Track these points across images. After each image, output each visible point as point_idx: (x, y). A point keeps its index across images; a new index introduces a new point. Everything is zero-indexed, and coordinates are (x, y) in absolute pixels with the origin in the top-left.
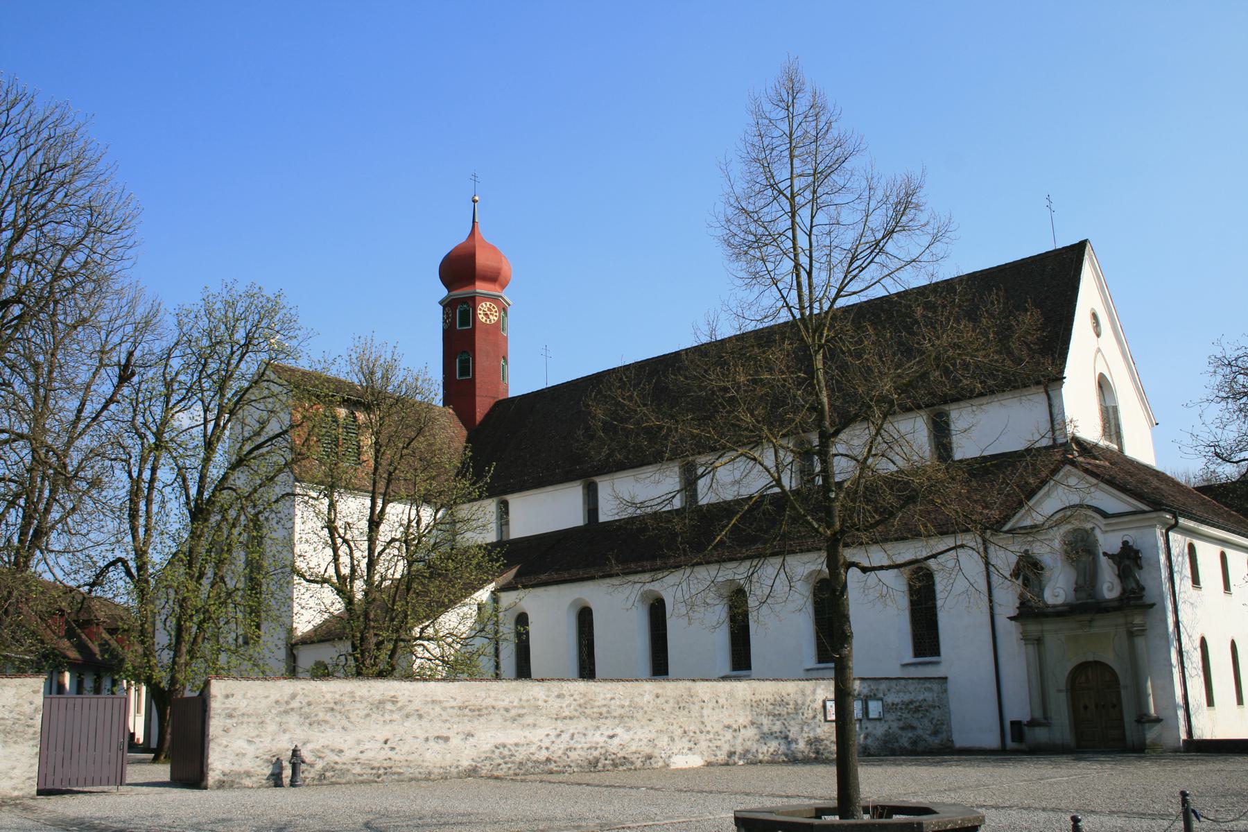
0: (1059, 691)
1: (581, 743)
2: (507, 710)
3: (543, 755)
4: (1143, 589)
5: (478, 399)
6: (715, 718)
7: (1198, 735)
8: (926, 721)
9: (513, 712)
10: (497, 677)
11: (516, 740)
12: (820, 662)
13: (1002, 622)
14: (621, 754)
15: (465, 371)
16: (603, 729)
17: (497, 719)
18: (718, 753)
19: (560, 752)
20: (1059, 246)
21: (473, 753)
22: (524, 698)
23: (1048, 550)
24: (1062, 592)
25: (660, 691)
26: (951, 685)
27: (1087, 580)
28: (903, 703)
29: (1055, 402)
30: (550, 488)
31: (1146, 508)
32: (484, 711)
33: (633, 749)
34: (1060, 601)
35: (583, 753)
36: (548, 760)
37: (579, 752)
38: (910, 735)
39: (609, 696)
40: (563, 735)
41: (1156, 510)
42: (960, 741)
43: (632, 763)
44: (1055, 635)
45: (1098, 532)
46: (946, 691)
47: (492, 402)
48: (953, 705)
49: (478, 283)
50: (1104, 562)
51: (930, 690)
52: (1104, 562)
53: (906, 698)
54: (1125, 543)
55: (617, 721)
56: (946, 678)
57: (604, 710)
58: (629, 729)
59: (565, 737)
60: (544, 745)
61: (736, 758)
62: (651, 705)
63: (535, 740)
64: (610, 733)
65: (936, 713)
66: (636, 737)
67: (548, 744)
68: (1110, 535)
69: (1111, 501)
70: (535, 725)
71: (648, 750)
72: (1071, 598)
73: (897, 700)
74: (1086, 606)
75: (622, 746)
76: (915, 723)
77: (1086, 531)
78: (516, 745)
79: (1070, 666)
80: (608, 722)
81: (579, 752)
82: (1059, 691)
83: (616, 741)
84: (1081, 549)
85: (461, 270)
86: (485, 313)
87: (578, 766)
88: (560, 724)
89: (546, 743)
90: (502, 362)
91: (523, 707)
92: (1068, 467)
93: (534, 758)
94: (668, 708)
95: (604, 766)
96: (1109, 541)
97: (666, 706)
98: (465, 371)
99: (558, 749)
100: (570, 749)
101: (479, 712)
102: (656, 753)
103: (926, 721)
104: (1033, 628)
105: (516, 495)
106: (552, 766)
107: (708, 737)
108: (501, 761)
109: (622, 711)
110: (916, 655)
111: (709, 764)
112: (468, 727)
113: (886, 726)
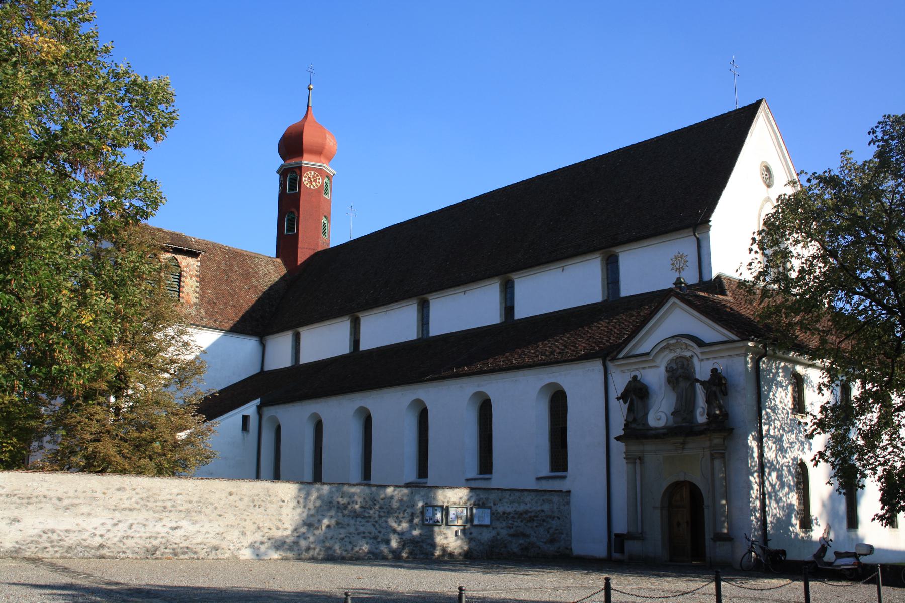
1: (143, 532)
2: (60, 499)
3: (97, 541)
5: (299, 251)
9: (66, 502)
10: (258, 477)
11: (68, 527)
12: (481, 473)
13: (613, 442)
14: (184, 544)
15: (291, 227)
16: (166, 521)
19: (116, 539)
21: (19, 537)
23: (654, 376)
24: (663, 416)
25: (234, 490)
26: (573, 499)
27: (685, 407)
28: (516, 512)
29: (703, 244)
30: (327, 322)
31: (735, 338)
32: (34, 500)
33: (199, 540)
34: (661, 423)
35: (141, 542)
36: (101, 546)
38: (521, 541)
39: (176, 491)
40: (120, 525)
41: (743, 340)
42: (578, 549)
43: (195, 553)
44: (655, 455)
45: (695, 360)
46: (568, 503)
47: (312, 253)
48: (574, 516)
49: (305, 156)
50: (699, 388)
51: (550, 501)
52: (699, 388)
53: (522, 508)
54: (715, 371)
55: (182, 515)
57: (169, 504)
58: (195, 522)
59: (123, 526)
60: (98, 532)
62: (222, 502)
63: (89, 528)
64: (174, 525)
65: (554, 523)
66: (203, 530)
68: (704, 363)
69: (709, 331)
70: (89, 514)
71: (215, 542)
72: (671, 422)
73: (509, 510)
74: (683, 429)
75: (186, 538)
77: (685, 358)
78: (67, 531)
79: (665, 485)
80: (173, 515)
81: (135, 540)
83: (180, 532)
84: (680, 375)
85: (292, 145)
86: (308, 181)
88: (117, 515)
90: (324, 220)
91: (77, 497)
92: (673, 300)
93: (85, 543)
94: (241, 505)
96: (702, 370)
97: (241, 505)
100: (127, 537)
101: (28, 500)
102: (224, 544)
105: (305, 328)
106: (104, 552)
108: (48, 545)
110: (552, 470)
112: (16, 513)
113: (494, 533)
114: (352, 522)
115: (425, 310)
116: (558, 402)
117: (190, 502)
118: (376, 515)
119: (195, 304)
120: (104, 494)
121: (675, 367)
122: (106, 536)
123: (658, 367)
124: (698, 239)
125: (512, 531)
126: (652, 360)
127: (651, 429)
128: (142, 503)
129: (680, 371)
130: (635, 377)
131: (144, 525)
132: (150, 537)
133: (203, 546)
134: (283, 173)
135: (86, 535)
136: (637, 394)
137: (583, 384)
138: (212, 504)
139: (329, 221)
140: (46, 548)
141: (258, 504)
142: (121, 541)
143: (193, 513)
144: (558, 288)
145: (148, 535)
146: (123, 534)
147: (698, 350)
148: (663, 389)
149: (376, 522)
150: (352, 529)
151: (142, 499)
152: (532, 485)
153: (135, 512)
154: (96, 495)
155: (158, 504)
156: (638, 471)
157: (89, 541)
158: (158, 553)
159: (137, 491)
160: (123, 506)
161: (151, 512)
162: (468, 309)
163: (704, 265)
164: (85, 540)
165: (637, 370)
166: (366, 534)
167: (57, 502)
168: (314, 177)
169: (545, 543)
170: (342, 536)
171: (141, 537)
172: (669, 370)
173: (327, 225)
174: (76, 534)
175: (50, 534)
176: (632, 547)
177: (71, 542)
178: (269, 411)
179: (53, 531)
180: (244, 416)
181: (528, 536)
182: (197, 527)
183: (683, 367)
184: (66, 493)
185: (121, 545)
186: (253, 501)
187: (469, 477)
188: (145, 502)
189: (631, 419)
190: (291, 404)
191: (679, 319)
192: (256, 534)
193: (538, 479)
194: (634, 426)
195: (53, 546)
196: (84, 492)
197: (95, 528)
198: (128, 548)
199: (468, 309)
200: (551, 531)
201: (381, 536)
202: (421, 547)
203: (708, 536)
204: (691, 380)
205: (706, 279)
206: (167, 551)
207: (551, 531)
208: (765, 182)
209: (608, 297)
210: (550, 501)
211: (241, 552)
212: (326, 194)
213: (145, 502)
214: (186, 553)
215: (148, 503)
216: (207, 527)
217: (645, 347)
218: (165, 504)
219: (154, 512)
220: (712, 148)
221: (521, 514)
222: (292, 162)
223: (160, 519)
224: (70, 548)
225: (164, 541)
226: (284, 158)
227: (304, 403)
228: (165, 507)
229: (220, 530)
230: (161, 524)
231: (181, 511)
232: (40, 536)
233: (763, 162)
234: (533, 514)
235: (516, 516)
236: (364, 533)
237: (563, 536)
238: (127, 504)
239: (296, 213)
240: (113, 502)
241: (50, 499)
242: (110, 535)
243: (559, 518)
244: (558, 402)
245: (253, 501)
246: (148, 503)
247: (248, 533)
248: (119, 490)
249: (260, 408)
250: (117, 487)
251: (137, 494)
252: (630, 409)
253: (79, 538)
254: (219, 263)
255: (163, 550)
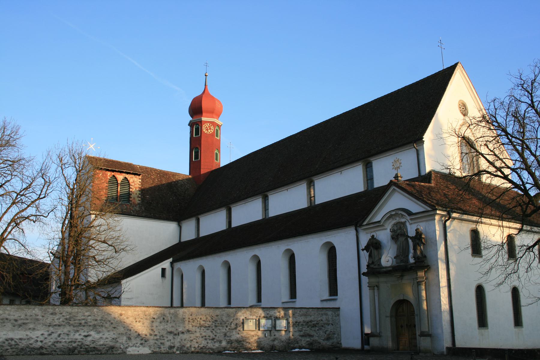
0: (387, 317)
1: (67, 339)
2: (16, 320)
3: (39, 344)
4: (425, 257)
6: (162, 327)
7: (460, 343)
8: (321, 332)
9: (20, 322)
11: (21, 337)
12: (291, 299)
14: (92, 346)
17: (9, 325)
18: (162, 346)
19: (50, 343)
20: (445, 68)
22: (28, 314)
23: (384, 235)
24: (390, 259)
26: (342, 313)
27: (402, 254)
28: (304, 321)
29: (420, 153)
31: (429, 209)
33: (101, 343)
34: (389, 264)
36: (41, 348)
37: (63, 344)
38: (308, 339)
45: (408, 224)
46: (338, 315)
49: (204, 114)
50: (410, 241)
51: (326, 314)
52: (410, 241)
53: (308, 319)
55: (91, 328)
56: (339, 308)
57: (83, 322)
58: (99, 332)
59: (55, 336)
61: (175, 350)
63: (34, 337)
64: (86, 334)
66: (104, 337)
67: (42, 339)
71: (111, 344)
75: (93, 342)
76: (312, 333)
77: (402, 223)
78: (21, 339)
79: (392, 302)
80: (85, 329)
81: (63, 344)
82: (387, 317)
83: (90, 339)
84: (399, 234)
85: (196, 109)
86: (206, 129)
87: (61, 350)
88: (51, 329)
89: (42, 338)
90: (216, 151)
91: (27, 319)
92: (393, 187)
93: (31, 346)
95: (79, 352)
98: (197, 157)
99: (50, 341)
100: (57, 342)
103: (321, 332)
104: (374, 280)
106: (44, 351)
107: (155, 338)
109: (96, 322)
111: (154, 353)
114: (198, 330)
115: (267, 201)
116: (331, 252)
117: (96, 320)
118: (213, 326)
119: (139, 204)
120: (43, 316)
121: (396, 229)
122: (44, 342)
123: (386, 229)
124: (417, 151)
125: (302, 333)
126: (382, 225)
127: (384, 268)
128: (66, 321)
129: (399, 231)
130: (373, 236)
131: (68, 335)
132: (71, 342)
133: (104, 346)
134: (191, 124)
135: (32, 341)
136: (374, 246)
137: (345, 241)
138: (110, 321)
139: (219, 152)
140: (7, 349)
141: (138, 320)
142: (53, 344)
143: (98, 327)
144: (341, 184)
145: (70, 340)
146: (55, 340)
147: (408, 218)
148: (390, 244)
149: (213, 329)
150: (198, 334)
151: (66, 319)
152: (319, 305)
153: (62, 327)
154: (38, 317)
155: (76, 322)
156: (376, 294)
157: (34, 345)
158: (76, 351)
159: (63, 314)
160: (55, 323)
161: (72, 327)
162: (288, 200)
163: (422, 165)
164: (31, 344)
165: (374, 231)
166: (207, 337)
167: (14, 322)
168: (209, 127)
169: (324, 340)
170: (192, 339)
171: (65, 342)
172: (393, 231)
173: (219, 154)
174: (26, 341)
175: (10, 341)
176: (374, 342)
177: (23, 345)
178: (177, 265)
179: (12, 339)
180: (162, 269)
181: (312, 336)
182: (101, 335)
183: (400, 228)
184: (20, 317)
185: (53, 347)
186: (136, 319)
187: (284, 301)
188: (68, 321)
189: (371, 263)
190: (188, 261)
191: (397, 201)
192: (137, 339)
193: (322, 301)
194: (372, 266)
195: (12, 349)
196: (31, 316)
197: (38, 337)
198: (57, 349)
199: (288, 200)
200: (327, 333)
201: (217, 338)
202: (243, 344)
203: (418, 333)
204: (405, 235)
205: (423, 174)
206: (82, 350)
207: (327, 333)
208: (462, 113)
209: (367, 188)
210: (326, 314)
211: (128, 350)
212: (217, 136)
213: (68, 321)
214: (94, 351)
215: (70, 322)
216: (107, 335)
217: (378, 218)
218: (80, 322)
219: (74, 326)
220: (427, 94)
221: (308, 322)
222: (196, 119)
223: (78, 331)
224: (22, 349)
225: (80, 344)
226: (192, 116)
227: (195, 260)
228: (80, 324)
229: (115, 336)
230: (78, 334)
231: (90, 326)
232: (4, 342)
233: (460, 101)
234: (315, 323)
235: (304, 324)
236: (205, 336)
237: (336, 336)
238: (57, 322)
239: (199, 148)
240: (49, 321)
241: (10, 320)
242: (47, 341)
243: (332, 324)
244: (331, 252)
245: (136, 319)
246: (70, 322)
247: (132, 338)
248: (52, 314)
249: (172, 263)
250: (50, 312)
251: (63, 316)
252: (370, 256)
253: (28, 343)
254: (154, 179)
255: (79, 349)
